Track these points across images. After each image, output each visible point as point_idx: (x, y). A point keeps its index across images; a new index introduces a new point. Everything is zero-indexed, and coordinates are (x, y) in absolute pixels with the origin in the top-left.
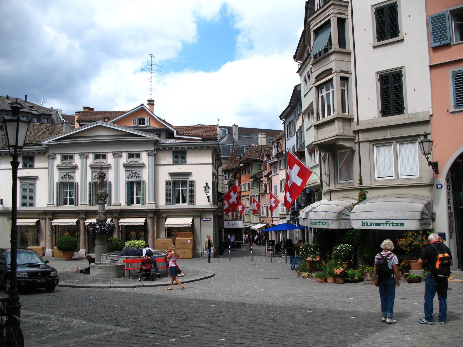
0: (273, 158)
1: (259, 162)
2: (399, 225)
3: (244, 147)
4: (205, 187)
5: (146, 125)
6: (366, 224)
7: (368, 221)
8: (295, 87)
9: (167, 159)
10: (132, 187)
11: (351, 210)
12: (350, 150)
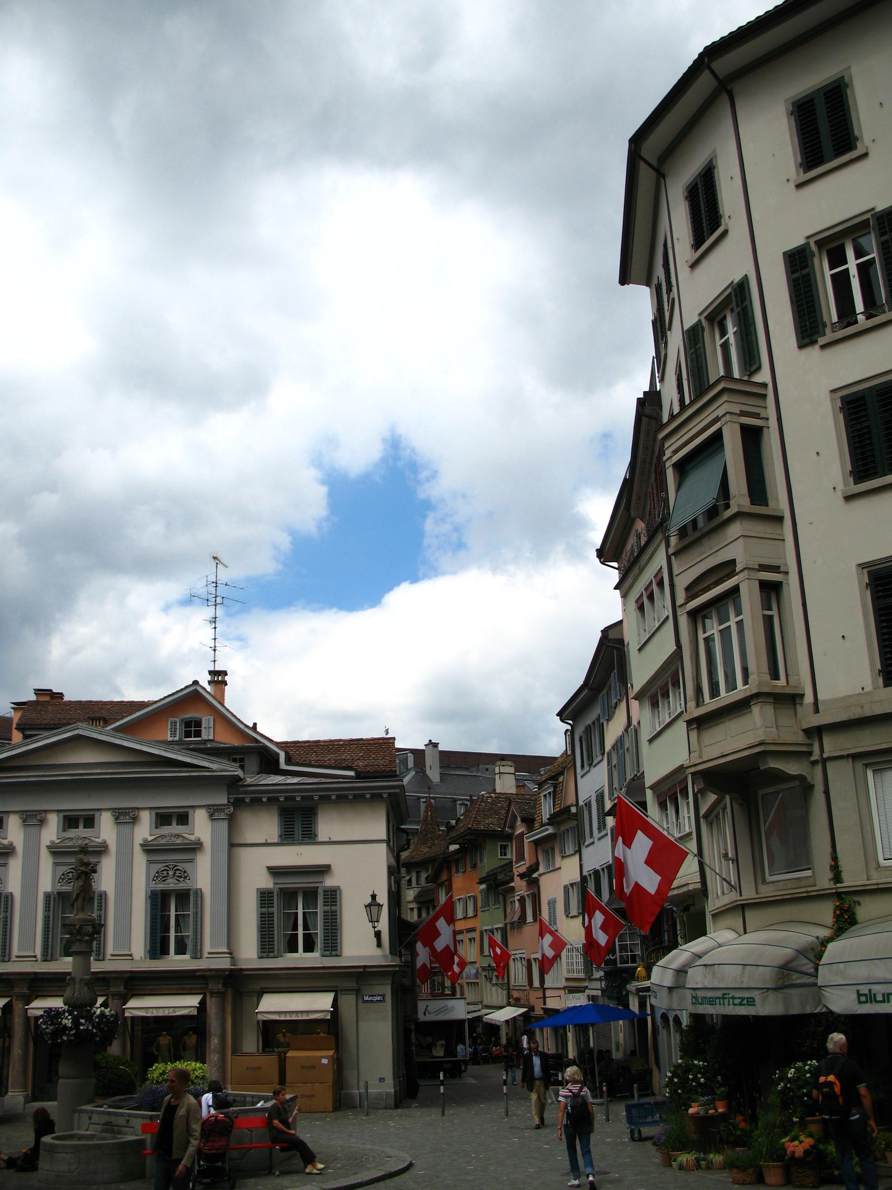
0: (542, 825)
1: (504, 837)
2: (745, 1002)
3: (455, 801)
5: (204, 736)
6: (871, 998)
7: (876, 988)
8: (605, 631)
9: (263, 827)
10: (165, 907)
11: (819, 957)
12: (797, 783)
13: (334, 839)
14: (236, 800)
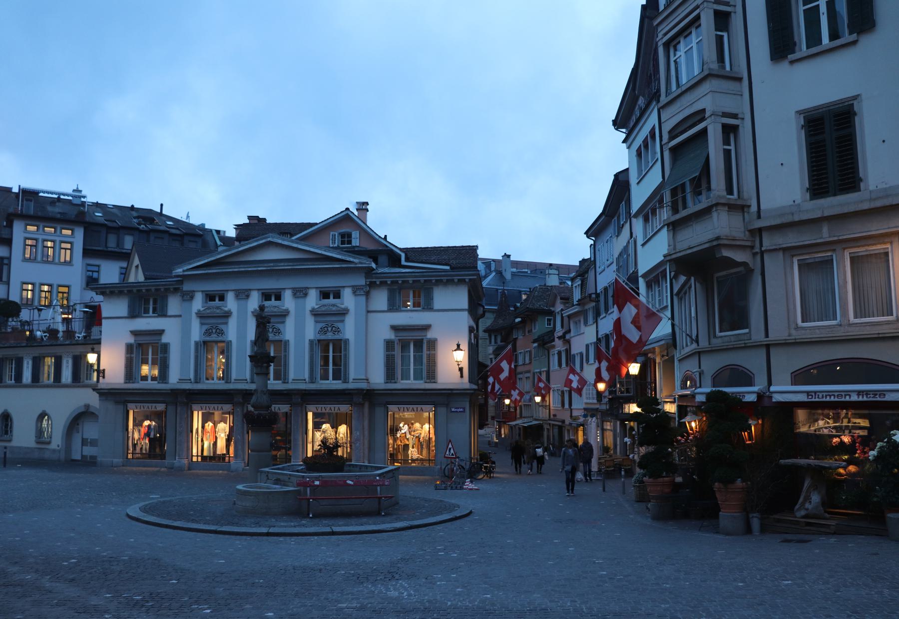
3: (520, 292)
5: (354, 244)
8: (617, 176)
12: (741, 269)
14: (371, 282)
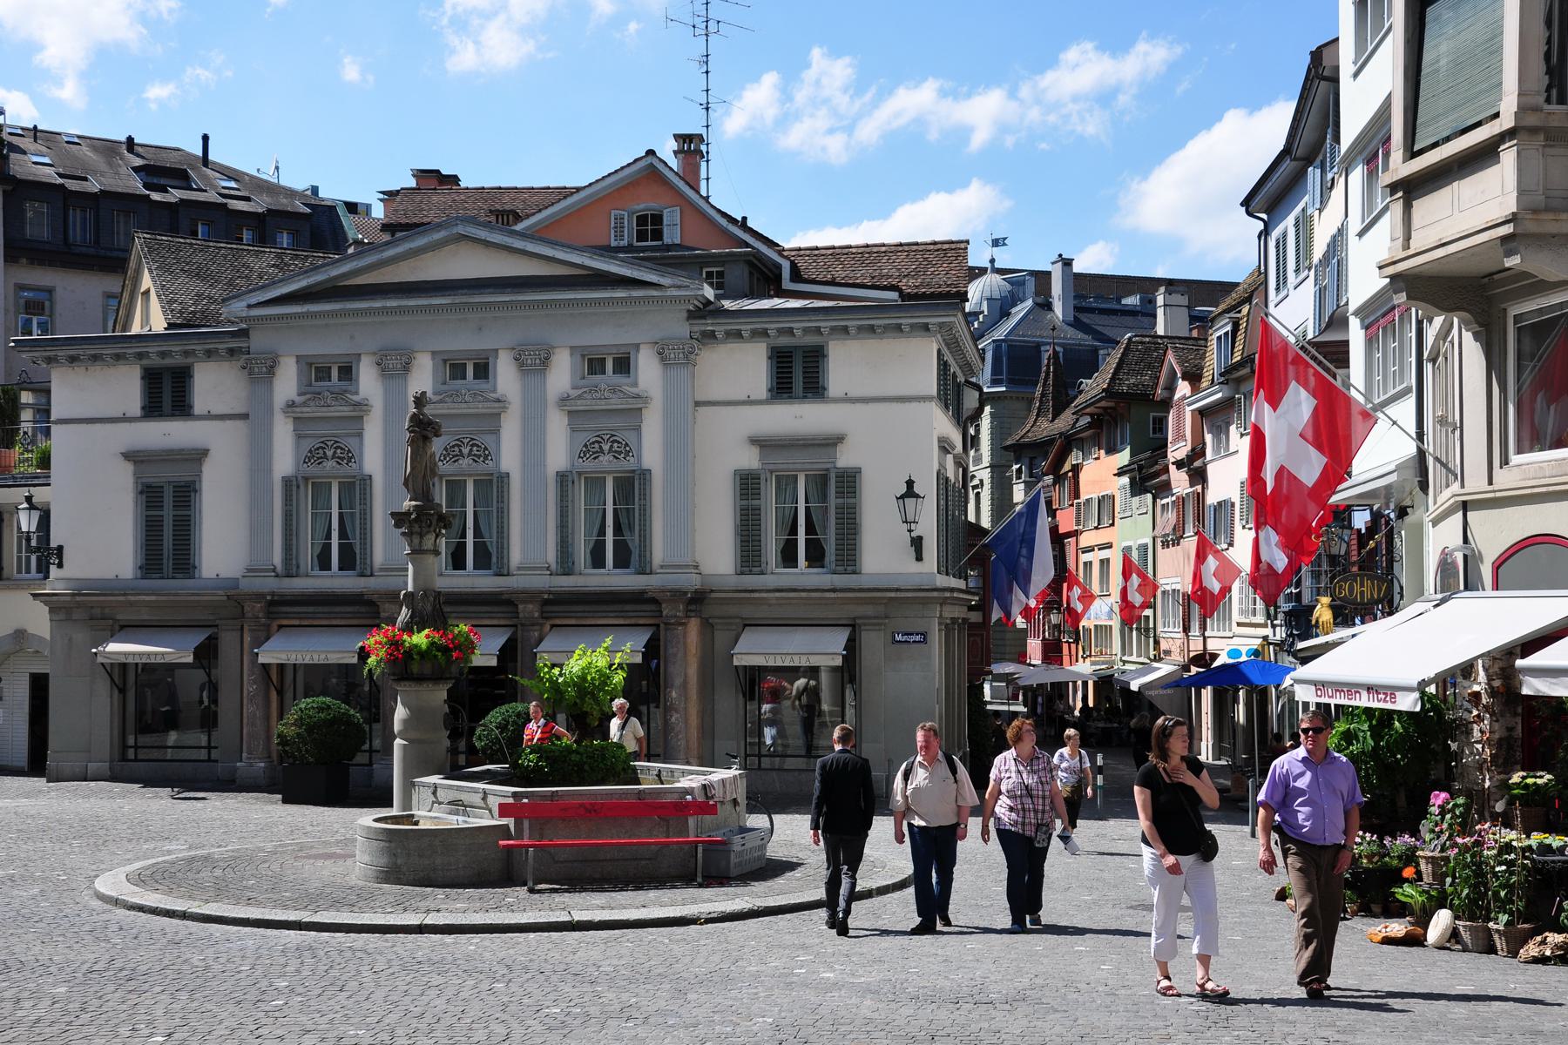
4: (902, 497)
5: (667, 240)
13: (853, 393)
